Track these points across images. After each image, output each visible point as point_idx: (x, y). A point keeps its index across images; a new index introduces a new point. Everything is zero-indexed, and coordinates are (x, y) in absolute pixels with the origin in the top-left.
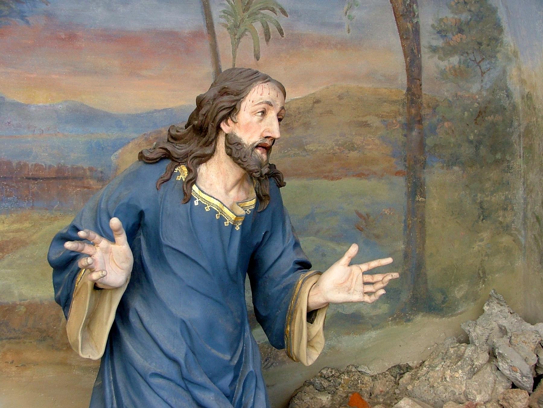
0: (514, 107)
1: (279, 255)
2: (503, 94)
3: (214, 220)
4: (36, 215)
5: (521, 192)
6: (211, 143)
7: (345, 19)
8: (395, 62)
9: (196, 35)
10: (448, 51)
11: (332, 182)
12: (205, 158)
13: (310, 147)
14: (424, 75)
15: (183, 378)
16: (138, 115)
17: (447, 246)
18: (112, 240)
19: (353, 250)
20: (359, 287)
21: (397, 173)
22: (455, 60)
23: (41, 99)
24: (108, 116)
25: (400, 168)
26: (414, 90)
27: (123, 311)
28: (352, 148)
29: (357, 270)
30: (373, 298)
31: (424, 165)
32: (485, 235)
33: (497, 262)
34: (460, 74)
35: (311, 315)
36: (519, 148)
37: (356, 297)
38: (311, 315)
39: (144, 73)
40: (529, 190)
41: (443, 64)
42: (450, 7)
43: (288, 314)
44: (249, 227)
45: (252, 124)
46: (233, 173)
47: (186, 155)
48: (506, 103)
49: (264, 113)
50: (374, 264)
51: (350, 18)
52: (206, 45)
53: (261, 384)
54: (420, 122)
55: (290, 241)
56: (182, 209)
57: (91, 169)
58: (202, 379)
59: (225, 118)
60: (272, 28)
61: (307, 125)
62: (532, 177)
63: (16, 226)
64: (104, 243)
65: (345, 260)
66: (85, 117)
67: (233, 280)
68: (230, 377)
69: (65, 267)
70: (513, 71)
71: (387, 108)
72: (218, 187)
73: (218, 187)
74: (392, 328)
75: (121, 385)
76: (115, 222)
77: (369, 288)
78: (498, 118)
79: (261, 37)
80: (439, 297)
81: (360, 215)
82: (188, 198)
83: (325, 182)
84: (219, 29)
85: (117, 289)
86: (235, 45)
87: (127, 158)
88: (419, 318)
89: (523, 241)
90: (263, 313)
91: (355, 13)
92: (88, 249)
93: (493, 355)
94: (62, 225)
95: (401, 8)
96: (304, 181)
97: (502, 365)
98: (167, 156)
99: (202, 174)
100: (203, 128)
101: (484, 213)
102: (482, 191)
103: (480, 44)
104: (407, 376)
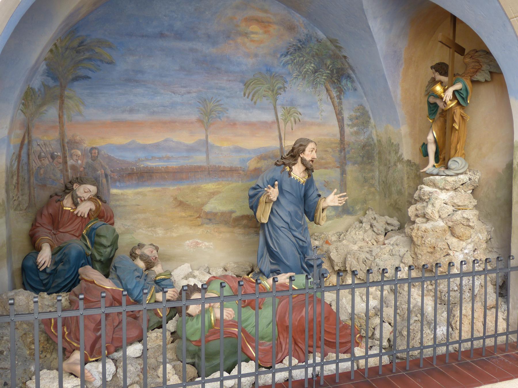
0: (375, 144)
2: (371, 140)
3: (298, 182)
4: (224, 183)
5: (377, 173)
6: (296, 160)
8: (336, 130)
9: (273, 122)
10: (353, 126)
11: (326, 170)
12: (294, 164)
14: (345, 134)
15: (289, 228)
19: (335, 190)
20: (337, 201)
21: (337, 167)
22: (355, 129)
25: (338, 165)
28: (323, 159)
30: (342, 204)
32: (366, 188)
34: (357, 133)
35: (323, 210)
36: (377, 158)
39: (257, 135)
40: (380, 172)
41: (352, 130)
43: (315, 210)
45: (309, 154)
46: (303, 168)
48: (372, 143)
50: (341, 195)
51: (322, 115)
52: (276, 126)
54: (344, 150)
56: (289, 179)
57: (241, 167)
58: (294, 228)
60: (297, 120)
62: (381, 168)
63: (217, 187)
64: (272, 189)
65: (333, 193)
66: (239, 150)
70: (374, 132)
71: (333, 145)
72: (298, 172)
73: (298, 172)
74: (336, 220)
77: (340, 202)
78: (370, 148)
79: (293, 122)
80: (351, 209)
82: (290, 175)
84: (280, 120)
86: (285, 126)
88: (345, 216)
89: (378, 190)
90: (307, 210)
91: (323, 114)
93: (371, 226)
95: (338, 112)
97: (375, 229)
98: (284, 164)
100: (295, 154)
102: (365, 173)
103: (363, 123)
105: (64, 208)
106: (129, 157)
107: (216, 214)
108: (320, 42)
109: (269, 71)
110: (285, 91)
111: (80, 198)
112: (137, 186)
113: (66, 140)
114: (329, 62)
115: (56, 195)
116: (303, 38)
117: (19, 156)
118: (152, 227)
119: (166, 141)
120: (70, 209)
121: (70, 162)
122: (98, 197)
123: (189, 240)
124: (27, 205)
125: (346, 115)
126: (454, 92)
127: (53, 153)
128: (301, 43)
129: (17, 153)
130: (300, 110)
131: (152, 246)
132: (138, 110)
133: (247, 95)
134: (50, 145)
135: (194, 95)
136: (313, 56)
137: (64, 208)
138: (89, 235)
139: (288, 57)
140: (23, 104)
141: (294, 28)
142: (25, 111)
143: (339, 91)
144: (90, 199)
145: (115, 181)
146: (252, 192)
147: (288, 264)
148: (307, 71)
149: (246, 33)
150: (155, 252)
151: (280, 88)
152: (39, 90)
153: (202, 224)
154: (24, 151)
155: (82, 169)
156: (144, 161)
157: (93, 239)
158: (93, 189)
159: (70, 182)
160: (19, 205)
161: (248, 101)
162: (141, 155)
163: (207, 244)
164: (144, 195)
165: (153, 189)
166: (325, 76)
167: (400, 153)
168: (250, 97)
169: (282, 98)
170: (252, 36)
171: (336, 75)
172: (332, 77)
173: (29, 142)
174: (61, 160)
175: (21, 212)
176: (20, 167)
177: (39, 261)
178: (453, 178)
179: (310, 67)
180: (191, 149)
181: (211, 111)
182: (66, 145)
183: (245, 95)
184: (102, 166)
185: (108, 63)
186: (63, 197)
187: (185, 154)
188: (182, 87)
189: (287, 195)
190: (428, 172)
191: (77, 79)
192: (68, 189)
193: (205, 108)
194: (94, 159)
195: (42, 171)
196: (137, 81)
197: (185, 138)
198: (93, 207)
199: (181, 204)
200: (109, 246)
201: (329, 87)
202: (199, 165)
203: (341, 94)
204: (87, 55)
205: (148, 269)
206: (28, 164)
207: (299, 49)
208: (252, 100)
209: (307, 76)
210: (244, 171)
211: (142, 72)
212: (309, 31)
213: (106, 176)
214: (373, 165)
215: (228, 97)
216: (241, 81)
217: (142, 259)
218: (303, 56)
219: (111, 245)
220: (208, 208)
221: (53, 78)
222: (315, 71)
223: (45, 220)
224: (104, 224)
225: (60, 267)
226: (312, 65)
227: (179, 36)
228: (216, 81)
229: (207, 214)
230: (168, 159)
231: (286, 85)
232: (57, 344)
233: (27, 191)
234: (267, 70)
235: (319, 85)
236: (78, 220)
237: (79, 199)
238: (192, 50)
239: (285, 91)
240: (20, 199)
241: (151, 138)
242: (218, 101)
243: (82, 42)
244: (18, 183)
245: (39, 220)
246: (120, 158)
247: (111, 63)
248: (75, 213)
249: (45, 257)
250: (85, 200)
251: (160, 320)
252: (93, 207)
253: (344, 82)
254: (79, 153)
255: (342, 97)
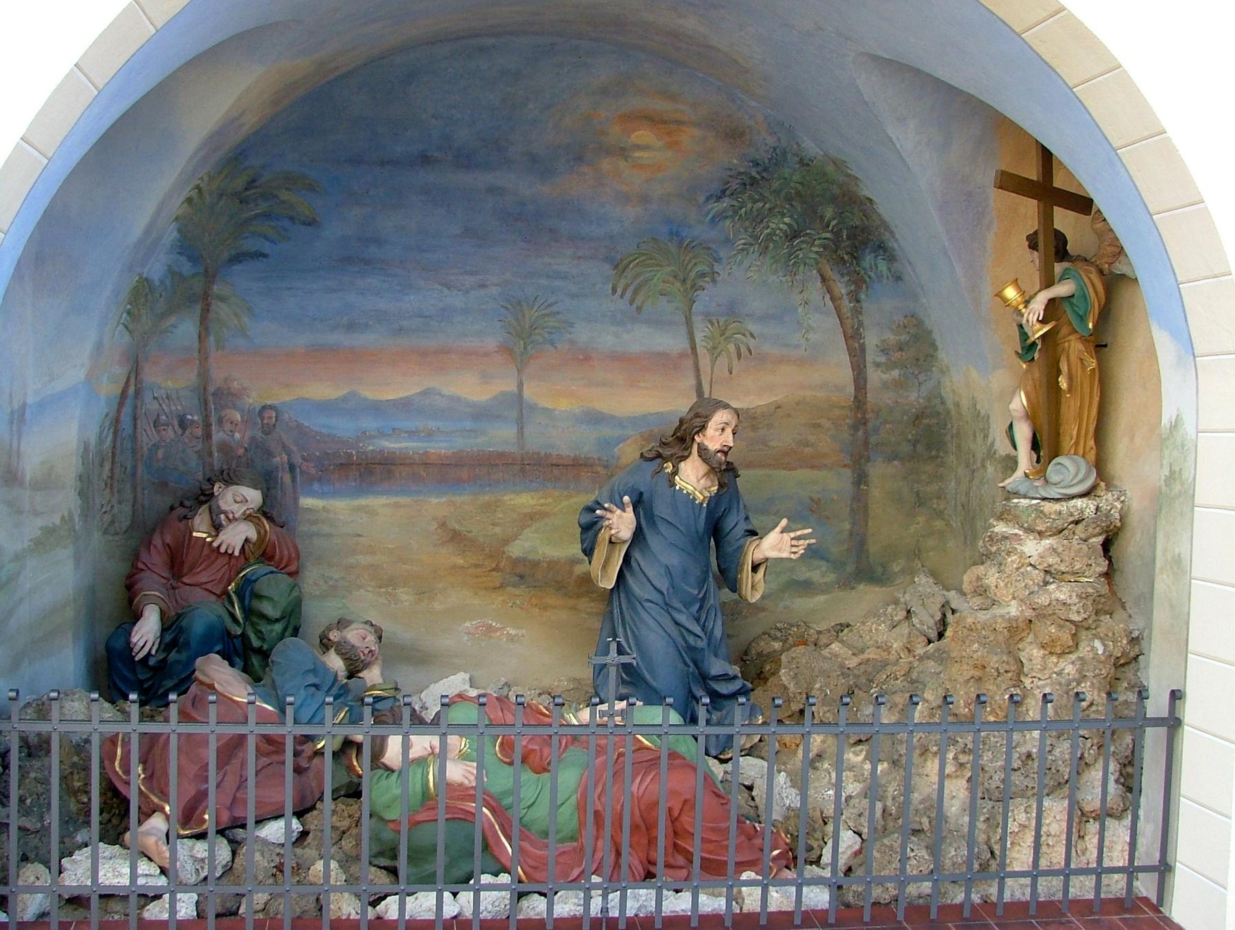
0: (948, 412)
1: (734, 524)
2: (937, 401)
3: (689, 499)
4: (557, 494)
7: (803, 342)
8: (845, 375)
9: (682, 355)
10: (889, 366)
12: (684, 458)
13: (772, 444)
16: (635, 418)
17: (887, 526)
18: (624, 511)
19: (784, 522)
21: (845, 466)
22: (896, 373)
23: (564, 405)
24: (613, 417)
25: (848, 462)
26: (860, 398)
27: (627, 558)
28: (807, 445)
29: (787, 537)
31: (868, 460)
32: (921, 519)
33: (931, 542)
34: (899, 385)
35: (755, 568)
37: (785, 555)
38: (755, 568)
39: (642, 385)
41: (885, 377)
42: (891, 329)
43: (739, 566)
44: (713, 504)
45: (716, 436)
46: (703, 468)
47: (672, 455)
48: (940, 409)
49: (723, 430)
50: (799, 533)
52: (689, 363)
53: (719, 614)
54: (865, 424)
55: (742, 515)
57: (599, 459)
58: (678, 605)
59: (697, 433)
60: (743, 349)
61: (770, 426)
63: (542, 501)
64: (619, 512)
65: (778, 529)
66: (595, 418)
67: (701, 540)
68: (697, 606)
69: (590, 528)
71: (837, 412)
72: (692, 478)
73: (692, 478)
75: (624, 607)
76: (626, 499)
77: (794, 549)
78: (934, 421)
79: (734, 356)
80: (880, 570)
81: (811, 499)
82: (673, 485)
83: (784, 472)
84: (700, 350)
85: (625, 542)
86: (713, 362)
87: (629, 452)
90: (723, 566)
91: (810, 336)
92: (609, 515)
94: (588, 499)
95: (850, 332)
96: (766, 471)
98: (659, 456)
99: (776, 272)
100: (682, 438)
101: (920, 501)
104: (846, 631)
105: (195, 534)
106: (344, 427)
107: (536, 564)
108: (808, 165)
109: (677, 234)
110: (714, 281)
111: (225, 513)
112: (359, 492)
113: (211, 389)
114: (829, 212)
115: (182, 505)
116: (763, 156)
117: (117, 421)
118: (387, 586)
119: (426, 393)
120: (204, 535)
121: (218, 436)
122: (265, 514)
123: (471, 620)
124: (128, 523)
125: (871, 340)
126: (1052, 302)
127: (185, 415)
128: (759, 169)
129: (113, 414)
130: (752, 327)
131: (367, 627)
132: (367, 325)
133: (619, 291)
134: (178, 398)
135: (495, 291)
136: (789, 199)
137: (195, 534)
138: (240, 593)
139: (726, 203)
140: (129, 313)
141: (742, 135)
142: (131, 327)
143: (855, 283)
144: (248, 517)
145: (311, 479)
146: (587, 518)
147: (654, 684)
148: (773, 234)
149: (623, 149)
150: (371, 638)
151: (703, 275)
152: (162, 282)
153: (502, 586)
154: (127, 410)
155: (241, 452)
156: (374, 437)
157: (247, 602)
158: (254, 496)
159: (209, 480)
160: (113, 522)
161: (622, 305)
162: (369, 423)
163: (512, 632)
164: (371, 512)
165: (393, 500)
166: (819, 246)
167: (990, 439)
168: (628, 295)
169: (706, 299)
170: (637, 154)
171: (848, 243)
172: (837, 248)
173: (138, 393)
174: (199, 432)
175: (117, 538)
176: (118, 443)
177: (134, 640)
178: (1057, 507)
179: (780, 224)
180: (482, 414)
181: (533, 327)
182: (210, 398)
183: (614, 290)
184: (284, 447)
185: (304, 223)
186: (193, 510)
187: (468, 425)
188: (466, 273)
189: (662, 527)
190: (1009, 488)
191: (237, 258)
192: (204, 497)
193: (517, 320)
194: (268, 430)
195: (160, 454)
196: (367, 262)
197: (469, 387)
198: (253, 534)
199: (455, 538)
200: (277, 620)
201: (829, 273)
202: (500, 449)
203: (859, 287)
204: (263, 207)
205: (351, 675)
206: (134, 438)
207: (754, 182)
208: (632, 302)
209: (771, 245)
210: (606, 467)
211: (378, 242)
212: (779, 139)
213: (292, 468)
214: (942, 464)
215: (573, 296)
216: (607, 259)
217: (338, 652)
218: (763, 199)
219: (283, 618)
220: (516, 550)
221: (190, 259)
222: (793, 235)
223: (156, 559)
224: (272, 572)
225: (173, 655)
226: (787, 220)
227: (465, 160)
228: (547, 260)
229: (516, 562)
230: (430, 435)
231: (717, 268)
232: (128, 802)
233: (128, 495)
234: (671, 233)
235: (802, 267)
236: (222, 561)
237: (222, 516)
238: (491, 190)
239: (714, 281)
240: (116, 510)
241: (394, 386)
242: (549, 306)
243: (254, 181)
244: (112, 478)
245: (144, 556)
246: (323, 431)
247: (311, 223)
248: (215, 544)
249: (147, 632)
250: (235, 519)
251: (356, 780)
252: (253, 534)
253: (868, 259)
254: (238, 417)
255: (863, 297)
